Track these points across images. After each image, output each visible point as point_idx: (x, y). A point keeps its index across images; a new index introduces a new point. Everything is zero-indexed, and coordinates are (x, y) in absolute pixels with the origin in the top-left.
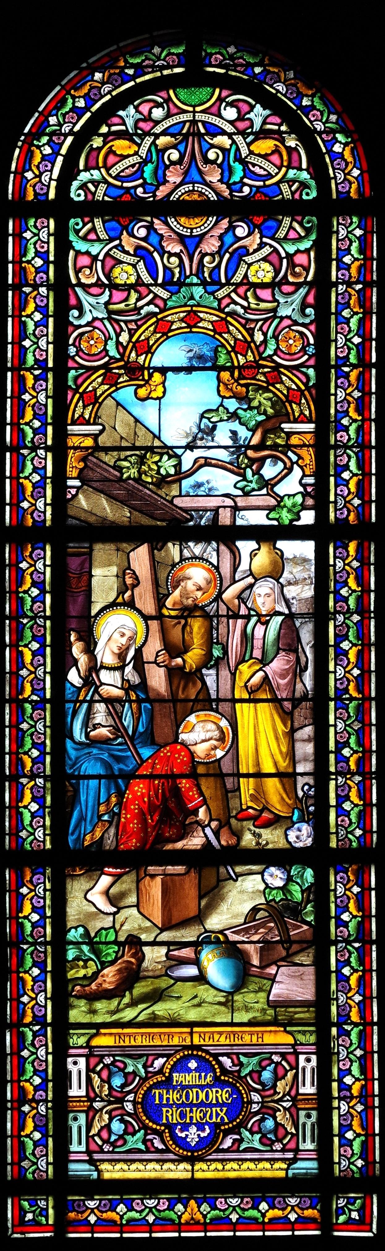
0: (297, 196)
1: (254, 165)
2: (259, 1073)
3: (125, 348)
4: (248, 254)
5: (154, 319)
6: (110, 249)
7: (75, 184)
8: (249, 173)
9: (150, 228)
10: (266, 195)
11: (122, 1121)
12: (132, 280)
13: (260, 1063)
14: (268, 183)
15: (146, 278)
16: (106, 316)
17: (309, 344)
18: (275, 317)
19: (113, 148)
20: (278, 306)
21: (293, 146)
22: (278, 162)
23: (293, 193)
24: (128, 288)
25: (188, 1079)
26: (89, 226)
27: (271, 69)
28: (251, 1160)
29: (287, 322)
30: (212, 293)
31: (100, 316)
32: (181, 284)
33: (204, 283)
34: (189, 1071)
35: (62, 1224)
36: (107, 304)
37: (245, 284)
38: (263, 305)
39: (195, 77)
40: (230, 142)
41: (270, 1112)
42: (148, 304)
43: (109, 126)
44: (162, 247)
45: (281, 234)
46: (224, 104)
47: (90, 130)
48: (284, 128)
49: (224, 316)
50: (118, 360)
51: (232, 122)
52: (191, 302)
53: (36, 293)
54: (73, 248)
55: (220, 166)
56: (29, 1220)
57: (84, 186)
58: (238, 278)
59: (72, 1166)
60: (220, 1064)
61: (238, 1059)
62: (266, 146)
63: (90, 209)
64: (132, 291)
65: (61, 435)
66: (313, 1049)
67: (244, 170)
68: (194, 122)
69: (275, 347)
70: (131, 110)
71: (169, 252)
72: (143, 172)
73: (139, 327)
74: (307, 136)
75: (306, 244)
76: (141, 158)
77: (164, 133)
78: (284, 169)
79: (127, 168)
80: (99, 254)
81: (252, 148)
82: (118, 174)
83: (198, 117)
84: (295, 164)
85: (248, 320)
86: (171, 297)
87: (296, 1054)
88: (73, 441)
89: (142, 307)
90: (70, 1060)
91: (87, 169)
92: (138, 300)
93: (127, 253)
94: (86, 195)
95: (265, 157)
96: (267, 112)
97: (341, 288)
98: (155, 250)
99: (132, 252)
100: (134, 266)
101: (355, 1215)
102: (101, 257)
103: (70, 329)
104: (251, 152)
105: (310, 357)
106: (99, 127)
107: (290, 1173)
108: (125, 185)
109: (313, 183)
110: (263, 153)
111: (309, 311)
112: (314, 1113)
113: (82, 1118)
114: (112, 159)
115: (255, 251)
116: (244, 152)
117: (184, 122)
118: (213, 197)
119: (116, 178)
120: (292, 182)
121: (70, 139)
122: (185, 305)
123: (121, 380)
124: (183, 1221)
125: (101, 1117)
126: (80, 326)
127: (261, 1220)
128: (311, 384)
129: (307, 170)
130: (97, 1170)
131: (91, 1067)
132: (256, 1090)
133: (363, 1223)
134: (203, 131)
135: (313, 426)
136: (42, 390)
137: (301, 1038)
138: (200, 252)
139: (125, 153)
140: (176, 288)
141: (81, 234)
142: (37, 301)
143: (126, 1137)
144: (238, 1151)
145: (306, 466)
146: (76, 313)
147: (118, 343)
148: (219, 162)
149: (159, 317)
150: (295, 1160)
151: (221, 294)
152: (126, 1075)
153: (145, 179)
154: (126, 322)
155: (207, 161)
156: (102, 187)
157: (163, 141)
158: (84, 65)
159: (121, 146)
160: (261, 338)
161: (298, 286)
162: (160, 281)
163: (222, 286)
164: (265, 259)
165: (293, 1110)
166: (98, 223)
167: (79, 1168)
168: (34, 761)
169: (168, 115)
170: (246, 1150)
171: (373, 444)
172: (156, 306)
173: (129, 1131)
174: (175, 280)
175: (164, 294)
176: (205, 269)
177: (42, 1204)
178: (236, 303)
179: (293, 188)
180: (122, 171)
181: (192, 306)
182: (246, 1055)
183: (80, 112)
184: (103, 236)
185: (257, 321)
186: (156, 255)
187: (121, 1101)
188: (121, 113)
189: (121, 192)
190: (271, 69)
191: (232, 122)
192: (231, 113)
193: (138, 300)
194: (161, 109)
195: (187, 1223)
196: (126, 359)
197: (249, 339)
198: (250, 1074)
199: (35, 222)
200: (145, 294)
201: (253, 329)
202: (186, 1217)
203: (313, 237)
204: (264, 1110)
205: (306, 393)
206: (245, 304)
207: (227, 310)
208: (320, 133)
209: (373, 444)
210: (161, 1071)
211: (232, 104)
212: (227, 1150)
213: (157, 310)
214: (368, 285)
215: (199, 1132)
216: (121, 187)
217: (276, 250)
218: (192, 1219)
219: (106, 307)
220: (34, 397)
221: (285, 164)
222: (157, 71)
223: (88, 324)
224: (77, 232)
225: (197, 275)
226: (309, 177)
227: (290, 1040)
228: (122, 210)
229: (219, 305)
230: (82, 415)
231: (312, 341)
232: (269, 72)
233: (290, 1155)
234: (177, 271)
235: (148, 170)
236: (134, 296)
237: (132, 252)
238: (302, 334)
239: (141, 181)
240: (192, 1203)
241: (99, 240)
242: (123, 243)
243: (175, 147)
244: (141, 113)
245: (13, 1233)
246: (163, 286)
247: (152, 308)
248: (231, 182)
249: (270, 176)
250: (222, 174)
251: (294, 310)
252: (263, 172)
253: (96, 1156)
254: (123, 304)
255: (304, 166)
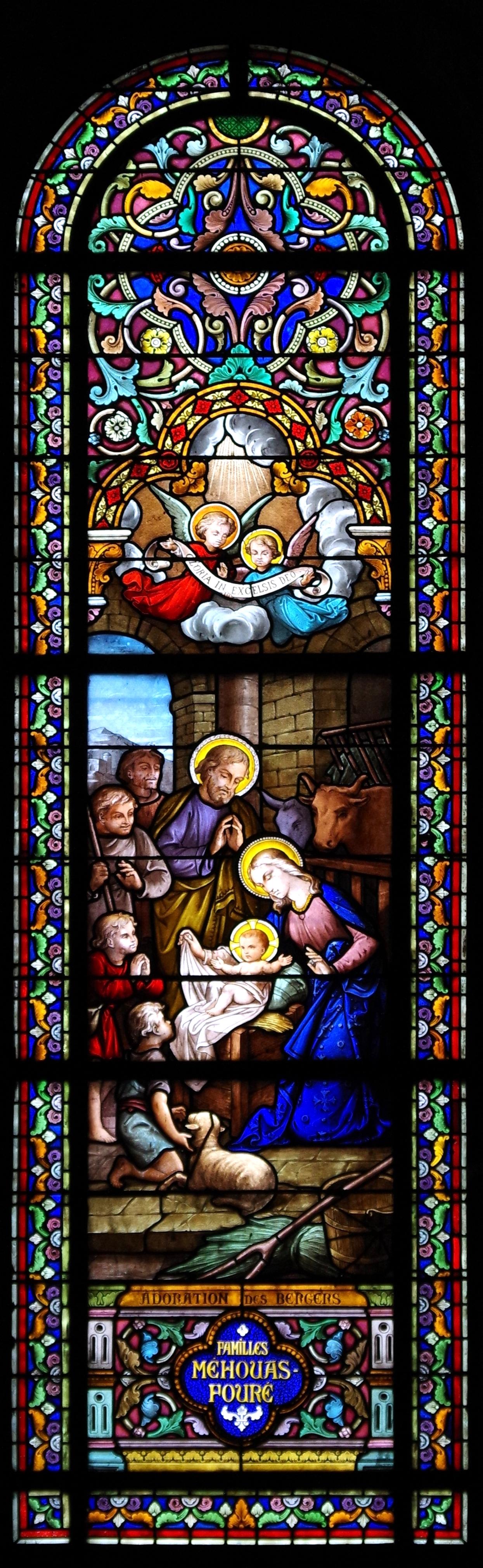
0: (364, 247)
1: (311, 211)
2: (324, 1343)
3: (159, 433)
4: (308, 318)
5: (193, 398)
6: (142, 309)
7: (95, 232)
8: (305, 220)
9: (189, 285)
10: (328, 247)
11: (157, 1400)
12: (165, 350)
13: (324, 1330)
14: (329, 231)
15: (186, 349)
16: (134, 394)
17: (382, 428)
18: (339, 395)
19: (142, 191)
20: (343, 381)
21: (358, 186)
22: (340, 206)
23: (360, 244)
24: (160, 359)
25: (235, 1347)
26: (114, 282)
27: (331, 94)
28: (313, 1449)
29: (352, 402)
30: (264, 366)
31: (128, 394)
32: (225, 354)
33: (254, 354)
34: (237, 1337)
35: (81, 1528)
36: (136, 379)
37: (302, 355)
38: (324, 380)
39: (240, 107)
40: (283, 182)
41: (337, 1390)
42: (185, 378)
43: (137, 163)
44: (204, 309)
45: (347, 294)
46: (274, 137)
47: (114, 166)
48: (345, 165)
49: (277, 393)
50: (149, 448)
51: (283, 158)
52: (240, 377)
53: (47, 364)
54: (93, 310)
55: (271, 212)
56: (40, 1524)
57: (105, 236)
58: (293, 348)
59: (94, 1456)
60: (275, 1329)
61: (299, 1324)
62: (325, 186)
63: (112, 263)
64: (166, 363)
65: (81, 543)
66: (388, 1312)
67: (300, 217)
68: (239, 159)
69: (340, 432)
70: (163, 143)
71: (211, 315)
72: (178, 218)
73: (175, 407)
74: (375, 175)
75: (376, 306)
76: (175, 201)
77: (204, 171)
78: (348, 215)
79: (158, 215)
80: (124, 319)
81: (308, 189)
82: (147, 223)
83: (247, 151)
84: (362, 208)
85: (307, 399)
86: (213, 371)
87: (369, 1319)
88: (96, 551)
89: (177, 383)
90: (92, 1324)
91: (110, 215)
92: (174, 373)
93: (161, 314)
94: (107, 247)
95: (324, 200)
96: (327, 146)
97: (421, 359)
98: (195, 312)
99: (166, 314)
100: (170, 331)
101: (441, 1519)
102: (127, 322)
103: (91, 409)
104: (308, 195)
105: (383, 443)
106: (126, 163)
107: (361, 1465)
108: (158, 235)
109: (383, 231)
110: (321, 195)
111: (380, 387)
112: (389, 1393)
113: (108, 1395)
114: (141, 203)
115: (317, 314)
116: (299, 194)
117: (228, 159)
118: (261, 247)
119: (146, 226)
120: (357, 232)
121: (89, 177)
122: (231, 380)
123: (152, 472)
124: (231, 1525)
125: (131, 1393)
126: (104, 407)
127: (324, 1525)
128: (383, 478)
129: (377, 216)
130: (124, 1458)
131: (119, 1332)
132: (320, 1365)
133: (451, 1529)
134: (249, 166)
135: (389, 529)
136: (57, 417)
137: (376, 1300)
138: (251, 314)
139: (156, 197)
140: (218, 360)
141: (102, 293)
142: (49, 508)
143: (160, 1420)
144: (297, 1437)
145: (379, 579)
146: (97, 389)
147: (150, 428)
148: (270, 206)
149: (200, 394)
150: (365, 1450)
151: (274, 366)
152: (160, 1343)
153: (180, 228)
154: (159, 401)
155: (255, 205)
156: (128, 239)
157: (203, 181)
158: (108, 86)
159: (152, 188)
160: (325, 421)
161: (369, 356)
162: (200, 351)
163: (276, 357)
164: (327, 324)
165: (364, 1389)
166: (124, 280)
167: (101, 1459)
168: (49, 336)
169: (209, 150)
170: (307, 1437)
171: (463, 550)
172: (196, 381)
173: (163, 1411)
174: (219, 349)
175: (205, 367)
176: (255, 336)
177: (56, 1504)
178: (293, 378)
179: (361, 238)
180: (153, 218)
181: (238, 382)
182: (307, 1320)
183: (101, 144)
184: (130, 294)
185: (318, 400)
186: (196, 318)
187: (154, 1375)
188: (150, 147)
189: (153, 242)
190: (331, 94)
191: (283, 158)
192: (281, 146)
193: (174, 373)
194: (198, 142)
195: (236, 1528)
196: (160, 447)
197: (310, 423)
198: (313, 1343)
199: (46, 278)
200: (180, 367)
201: (314, 410)
202: (233, 1520)
203: (386, 297)
204: (329, 1388)
205: (379, 489)
206: (303, 378)
207: (281, 386)
208: (393, 170)
209: (463, 550)
210: (202, 1339)
211: (283, 136)
212: (286, 1437)
213: (196, 386)
214: (453, 354)
215: (250, 1415)
216: (153, 237)
217: (341, 314)
218: (241, 1522)
219: (135, 384)
220: (47, 494)
221: (350, 205)
222: (194, 95)
223: (112, 405)
224: (98, 291)
225: (245, 344)
226: (379, 223)
227: (360, 1300)
228: (153, 264)
229: (272, 380)
230: (104, 517)
231: (385, 424)
232: (329, 97)
233: (358, 1443)
234: (220, 340)
235: (185, 215)
236: (169, 367)
237: (166, 314)
238: (371, 414)
239: (176, 230)
240: (241, 1504)
241: (124, 300)
242: (156, 303)
243: (216, 188)
244: (175, 148)
245: (20, 1538)
246: (204, 357)
247: (190, 384)
248: (285, 231)
249: (332, 224)
250: (274, 222)
251: (362, 386)
252: (321, 219)
253: (123, 1443)
254: (156, 378)
255: (372, 212)
